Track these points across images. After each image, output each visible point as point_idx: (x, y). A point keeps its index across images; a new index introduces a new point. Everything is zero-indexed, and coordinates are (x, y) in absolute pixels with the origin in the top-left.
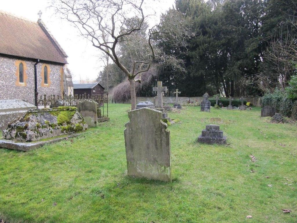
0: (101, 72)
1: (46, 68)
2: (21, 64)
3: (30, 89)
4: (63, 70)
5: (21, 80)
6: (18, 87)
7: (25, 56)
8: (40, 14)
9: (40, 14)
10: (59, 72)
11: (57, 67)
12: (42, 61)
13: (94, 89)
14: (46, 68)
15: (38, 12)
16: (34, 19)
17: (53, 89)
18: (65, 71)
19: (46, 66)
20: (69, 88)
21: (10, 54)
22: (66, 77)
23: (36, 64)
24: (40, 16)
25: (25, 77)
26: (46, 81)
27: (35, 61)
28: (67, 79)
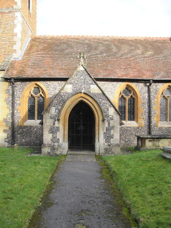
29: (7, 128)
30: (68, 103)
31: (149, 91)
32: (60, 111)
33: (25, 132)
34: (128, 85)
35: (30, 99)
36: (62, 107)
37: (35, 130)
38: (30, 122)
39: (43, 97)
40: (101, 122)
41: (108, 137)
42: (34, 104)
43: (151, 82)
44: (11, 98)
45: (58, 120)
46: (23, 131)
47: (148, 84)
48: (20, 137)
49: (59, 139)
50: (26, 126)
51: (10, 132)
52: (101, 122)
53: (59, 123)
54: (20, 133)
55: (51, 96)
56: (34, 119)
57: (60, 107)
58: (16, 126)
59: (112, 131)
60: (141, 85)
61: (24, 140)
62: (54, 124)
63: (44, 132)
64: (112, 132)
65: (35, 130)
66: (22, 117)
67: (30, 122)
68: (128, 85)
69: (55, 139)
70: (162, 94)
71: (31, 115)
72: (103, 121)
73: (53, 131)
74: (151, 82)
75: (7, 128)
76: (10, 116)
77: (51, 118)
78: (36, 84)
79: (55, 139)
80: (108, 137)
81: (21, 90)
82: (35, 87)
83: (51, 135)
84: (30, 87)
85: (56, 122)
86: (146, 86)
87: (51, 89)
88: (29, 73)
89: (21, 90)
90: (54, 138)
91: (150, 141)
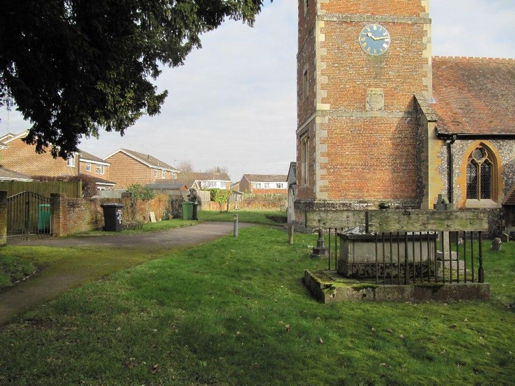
39: (489, 164)
44: (446, 166)
56: (475, 198)
78: (482, 144)
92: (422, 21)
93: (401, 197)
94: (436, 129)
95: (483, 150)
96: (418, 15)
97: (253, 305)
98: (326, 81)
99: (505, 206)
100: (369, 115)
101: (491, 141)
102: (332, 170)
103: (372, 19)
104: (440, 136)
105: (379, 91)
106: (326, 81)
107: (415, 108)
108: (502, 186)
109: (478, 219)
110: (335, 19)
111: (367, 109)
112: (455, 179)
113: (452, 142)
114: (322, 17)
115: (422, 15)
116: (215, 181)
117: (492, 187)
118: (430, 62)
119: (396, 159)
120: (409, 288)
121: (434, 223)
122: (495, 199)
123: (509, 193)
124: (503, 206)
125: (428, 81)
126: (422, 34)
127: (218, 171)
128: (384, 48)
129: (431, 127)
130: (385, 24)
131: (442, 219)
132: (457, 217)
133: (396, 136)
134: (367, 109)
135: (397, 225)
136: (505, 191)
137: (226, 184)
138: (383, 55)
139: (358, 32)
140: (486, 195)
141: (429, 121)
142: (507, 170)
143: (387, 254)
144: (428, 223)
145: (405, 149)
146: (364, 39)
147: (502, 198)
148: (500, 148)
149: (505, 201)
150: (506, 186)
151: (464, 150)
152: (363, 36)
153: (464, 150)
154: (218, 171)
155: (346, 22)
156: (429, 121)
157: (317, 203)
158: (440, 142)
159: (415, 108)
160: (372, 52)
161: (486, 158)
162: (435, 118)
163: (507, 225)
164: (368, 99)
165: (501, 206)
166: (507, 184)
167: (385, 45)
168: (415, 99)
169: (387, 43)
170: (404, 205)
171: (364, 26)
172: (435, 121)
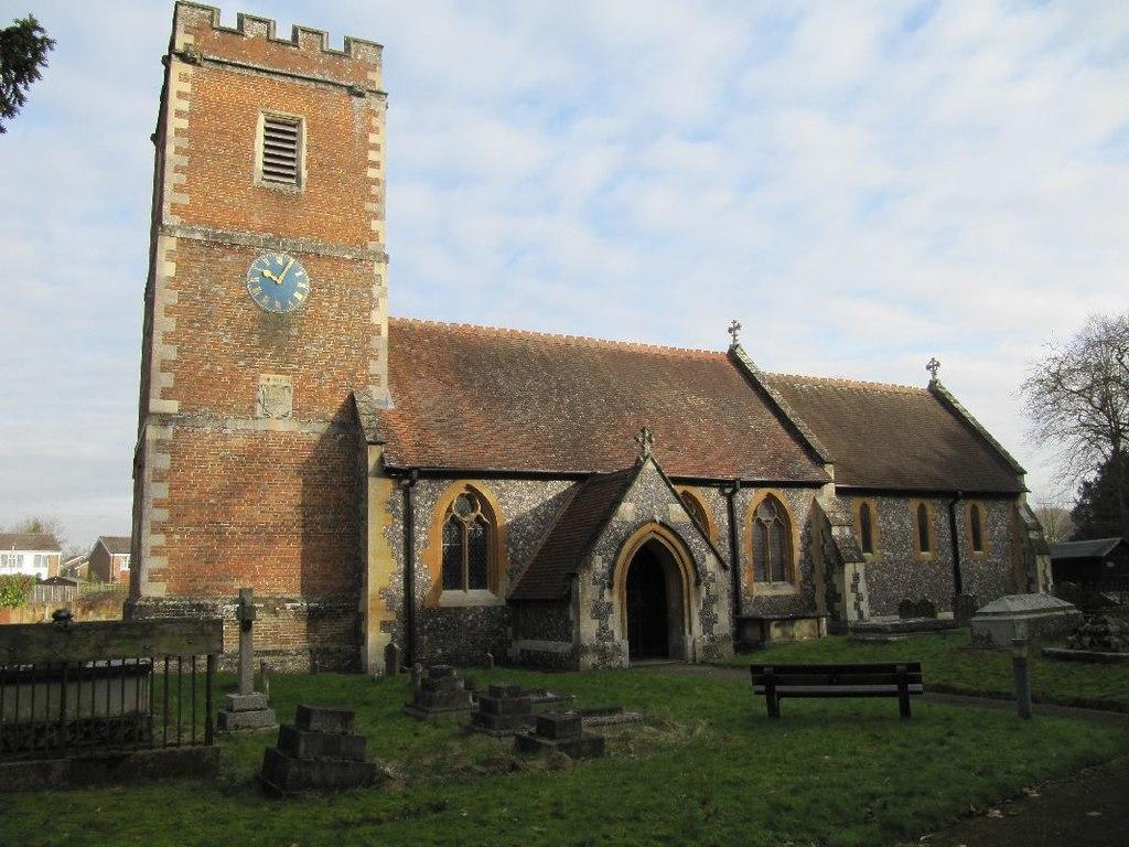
0: (1087, 485)
1: (974, 510)
2: (922, 509)
3: (943, 566)
4: (1016, 509)
5: (924, 547)
6: (918, 564)
7: (930, 487)
8: (933, 366)
9: (933, 366)
10: (1009, 515)
11: (1001, 505)
12: (969, 495)
13: (1109, 557)
14: (974, 510)
15: (390, 260)
16: (719, 345)
17: (997, 565)
18: (1023, 513)
19: (974, 506)
20: (1039, 560)
21: (899, 486)
22: (1028, 529)
23: (953, 504)
24: (934, 374)
25: (932, 537)
26: (977, 546)
27: (950, 497)
28: (1033, 535)
29: (391, 617)
30: (628, 546)
31: (731, 509)
32: (613, 564)
33: (443, 625)
34: (769, 495)
35: (448, 528)
36: (617, 553)
37: (470, 618)
38: (451, 597)
39: (483, 524)
40: (692, 589)
41: (709, 622)
42: (461, 542)
43: (738, 486)
44: (402, 527)
45: (611, 586)
46: (436, 622)
47: (728, 491)
48: (430, 641)
49: (612, 632)
50: (446, 608)
51: (398, 629)
52: (692, 589)
53: (611, 594)
54: (429, 629)
55: (509, 520)
56: (458, 588)
57: (611, 556)
58: (418, 606)
59: (715, 606)
60: (714, 491)
61: (440, 651)
62: (602, 596)
63: (582, 617)
64: (715, 607)
65: (470, 618)
66: (433, 583)
67: (451, 597)
68: (769, 495)
69: (604, 633)
70: (755, 513)
71: (451, 577)
72: (698, 583)
73: (601, 613)
74: (738, 486)
75: (391, 617)
76: (399, 581)
77: (595, 583)
78: (469, 487)
79: (604, 633)
80: (709, 622)
81: (429, 503)
82: (462, 495)
83: (596, 623)
84: (455, 489)
85: (606, 591)
86: (724, 494)
87: (510, 502)
88: (447, 452)
89: (429, 503)
90: (604, 628)
91: (776, 626)
92: (371, 258)
93: (323, 588)
94: (382, 459)
95: (472, 497)
96: (364, 247)
97: (241, 824)
98: (173, 356)
99: (514, 603)
100: (261, 426)
101: (485, 481)
102: (178, 537)
103: (273, 244)
104: (386, 472)
105: (284, 380)
106: (173, 356)
107: (349, 418)
108: (505, 563)
109: (203, 634)
110: (198, 236)
111: (258, 414)
112: (419, 552)
113: (412, 484)
114: (172, 229)
115: (371, 246)
116: (20, 552)
117: (927, 545)
118: (385, 332)
119: (313, 514)
120: (59, 766)
121: (119, 645)
122: (495, 590)
123: (519, 577)
124: (508, 601)
125: (380, 366)
126: (370, 280)
127: (37, 527)
128: (295, 300)
129: (373, 456)
130: (302, 256)
131: (135, 637)
132: (163, 633)
133: (315, 469)
134: (258, 414)
135: (45, 652)
136: (512, 574)
137: (50, 562)
138: (294, 313)
139: (245, 266)
140: (479, 581)
141: (370, 443)
142: (513, 535)
143: (55, 707)
144: (108, 646)
145: (334, 494)
146: (257, 279)
147: (506, 586)
148: (501, 496)
149: (511, 593)
150: (512, 563)
151: (437, 505)
152: (254, 274)
153: (437, 505)
154: (37, 527)
155: (220, 245)
156: (370, 443)
157: (140, 606)
158: (389, 484)
159: (349, 418)
160: (272, 305)
161: (479, 512)
162: (381, 436)
163: (516, 638)
164: (260, 395)
165: (504, 602)
166: (514, 561)
167: (298, 295)
168: (352, 400)
169: (302, 291)
170: (328, 605)
171: (258, 254)
172: (381, 443)
